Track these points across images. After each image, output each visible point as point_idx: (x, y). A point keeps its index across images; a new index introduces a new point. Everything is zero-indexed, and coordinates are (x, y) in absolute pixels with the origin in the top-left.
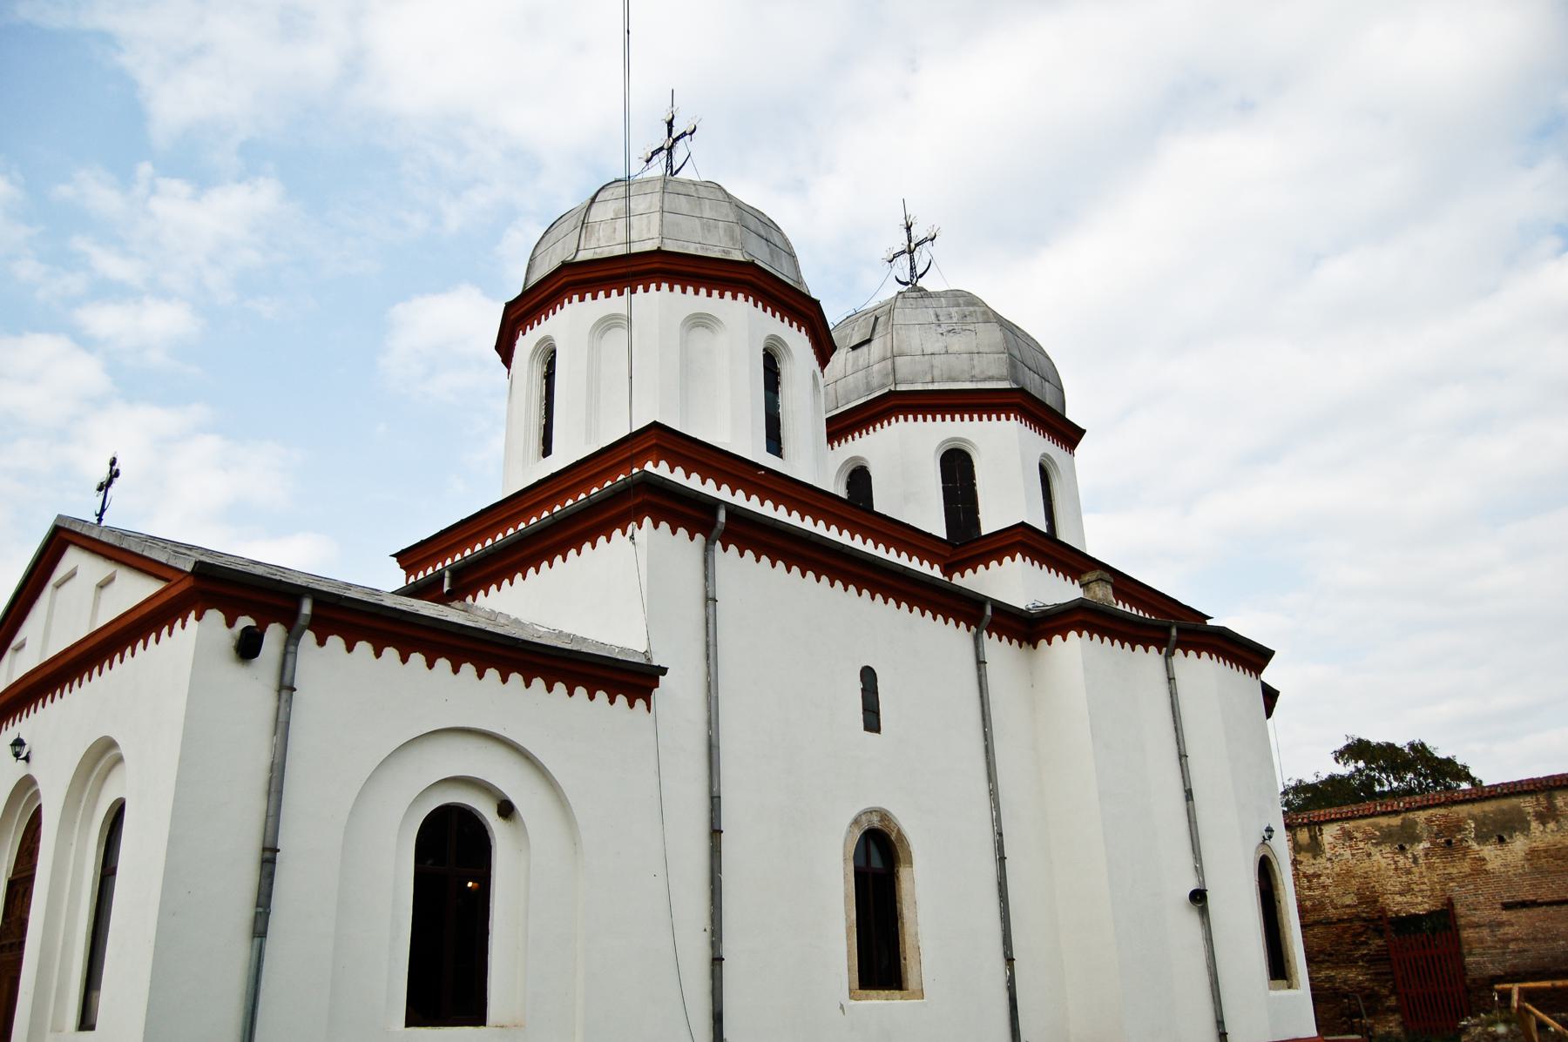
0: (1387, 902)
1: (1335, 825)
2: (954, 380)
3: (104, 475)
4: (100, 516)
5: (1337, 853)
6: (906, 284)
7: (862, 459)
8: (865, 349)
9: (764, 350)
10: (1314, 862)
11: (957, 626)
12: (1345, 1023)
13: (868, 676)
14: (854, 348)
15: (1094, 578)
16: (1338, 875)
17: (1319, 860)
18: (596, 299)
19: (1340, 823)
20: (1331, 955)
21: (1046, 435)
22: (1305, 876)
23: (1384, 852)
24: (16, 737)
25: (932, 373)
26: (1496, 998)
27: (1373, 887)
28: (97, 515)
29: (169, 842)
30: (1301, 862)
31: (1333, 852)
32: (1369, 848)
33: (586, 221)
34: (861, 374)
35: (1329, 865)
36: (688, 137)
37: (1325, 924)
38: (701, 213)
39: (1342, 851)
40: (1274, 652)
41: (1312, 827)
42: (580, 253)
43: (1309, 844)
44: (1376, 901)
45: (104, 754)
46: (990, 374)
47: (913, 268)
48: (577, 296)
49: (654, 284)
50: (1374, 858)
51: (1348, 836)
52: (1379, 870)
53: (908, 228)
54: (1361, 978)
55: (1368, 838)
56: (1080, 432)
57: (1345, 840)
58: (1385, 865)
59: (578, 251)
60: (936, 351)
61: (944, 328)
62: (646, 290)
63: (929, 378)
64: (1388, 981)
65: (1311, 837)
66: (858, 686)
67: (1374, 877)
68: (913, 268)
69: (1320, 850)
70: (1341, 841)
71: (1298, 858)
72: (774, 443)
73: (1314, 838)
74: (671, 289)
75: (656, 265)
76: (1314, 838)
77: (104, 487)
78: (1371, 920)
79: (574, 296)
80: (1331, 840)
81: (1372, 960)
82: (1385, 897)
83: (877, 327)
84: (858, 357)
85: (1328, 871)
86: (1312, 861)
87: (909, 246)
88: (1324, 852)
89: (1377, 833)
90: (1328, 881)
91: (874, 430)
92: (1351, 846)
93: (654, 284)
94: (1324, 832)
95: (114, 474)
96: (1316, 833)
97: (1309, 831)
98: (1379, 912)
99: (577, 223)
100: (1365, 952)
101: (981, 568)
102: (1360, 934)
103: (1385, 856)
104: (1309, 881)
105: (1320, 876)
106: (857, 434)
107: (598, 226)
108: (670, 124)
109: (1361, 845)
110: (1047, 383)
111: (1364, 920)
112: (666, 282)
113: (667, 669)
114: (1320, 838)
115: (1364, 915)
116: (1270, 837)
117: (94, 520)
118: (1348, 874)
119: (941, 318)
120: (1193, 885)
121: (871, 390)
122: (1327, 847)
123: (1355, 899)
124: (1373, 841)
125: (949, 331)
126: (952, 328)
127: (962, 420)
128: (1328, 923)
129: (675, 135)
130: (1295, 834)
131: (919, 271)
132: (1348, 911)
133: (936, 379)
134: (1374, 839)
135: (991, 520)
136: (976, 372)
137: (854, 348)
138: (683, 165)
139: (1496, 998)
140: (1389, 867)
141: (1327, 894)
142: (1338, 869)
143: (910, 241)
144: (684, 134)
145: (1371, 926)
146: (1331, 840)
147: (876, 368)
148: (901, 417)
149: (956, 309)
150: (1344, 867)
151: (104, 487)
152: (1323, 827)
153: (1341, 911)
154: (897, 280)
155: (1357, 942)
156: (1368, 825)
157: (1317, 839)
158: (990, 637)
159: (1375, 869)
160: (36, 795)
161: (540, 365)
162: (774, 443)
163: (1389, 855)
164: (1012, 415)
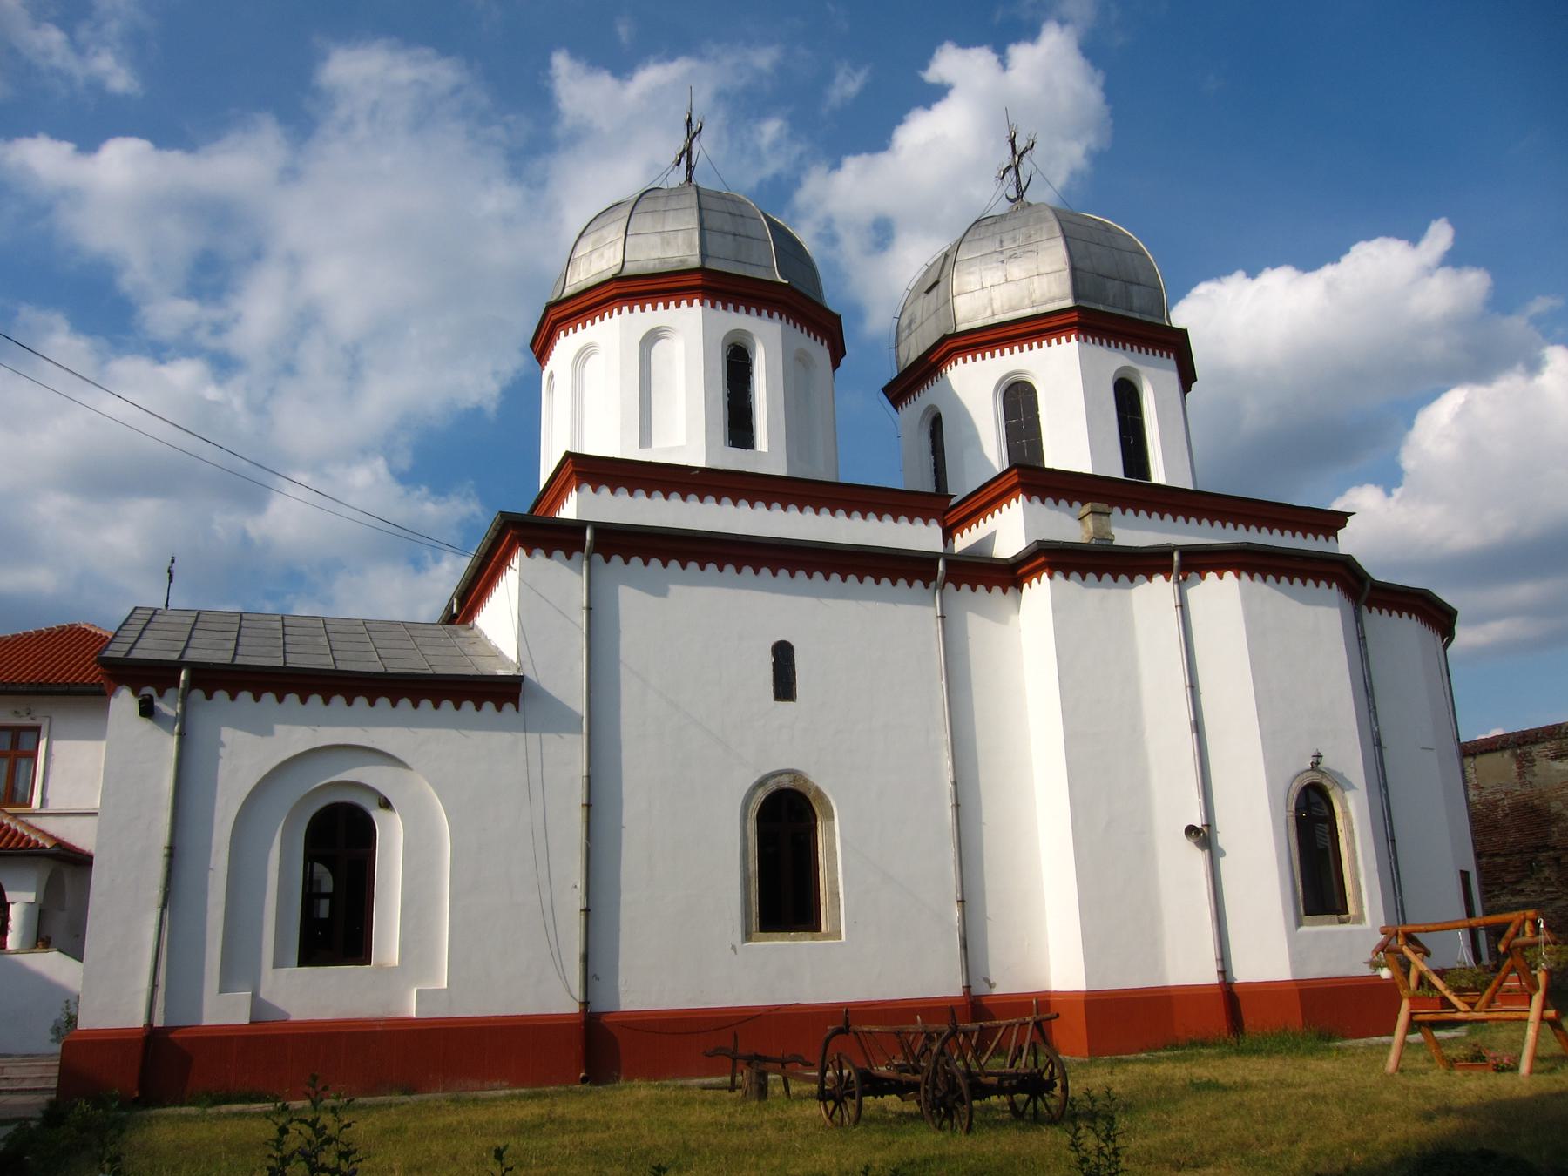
4: (167, 605)
15: (1086, 512)
26: (1542, 926)
36: (1028, 152)
46: (1052, 295)
63: (989, 312)
66: (769, 660)
68: (1018, 183)
75: (614, 292)
79: (624, 308)
108: (1013, 142)
110: (1135, 288)
116: (1318, 763)
117: (164, 607)
139: (1542, 926)
143: (1014, 152)
164: (1073, 336)
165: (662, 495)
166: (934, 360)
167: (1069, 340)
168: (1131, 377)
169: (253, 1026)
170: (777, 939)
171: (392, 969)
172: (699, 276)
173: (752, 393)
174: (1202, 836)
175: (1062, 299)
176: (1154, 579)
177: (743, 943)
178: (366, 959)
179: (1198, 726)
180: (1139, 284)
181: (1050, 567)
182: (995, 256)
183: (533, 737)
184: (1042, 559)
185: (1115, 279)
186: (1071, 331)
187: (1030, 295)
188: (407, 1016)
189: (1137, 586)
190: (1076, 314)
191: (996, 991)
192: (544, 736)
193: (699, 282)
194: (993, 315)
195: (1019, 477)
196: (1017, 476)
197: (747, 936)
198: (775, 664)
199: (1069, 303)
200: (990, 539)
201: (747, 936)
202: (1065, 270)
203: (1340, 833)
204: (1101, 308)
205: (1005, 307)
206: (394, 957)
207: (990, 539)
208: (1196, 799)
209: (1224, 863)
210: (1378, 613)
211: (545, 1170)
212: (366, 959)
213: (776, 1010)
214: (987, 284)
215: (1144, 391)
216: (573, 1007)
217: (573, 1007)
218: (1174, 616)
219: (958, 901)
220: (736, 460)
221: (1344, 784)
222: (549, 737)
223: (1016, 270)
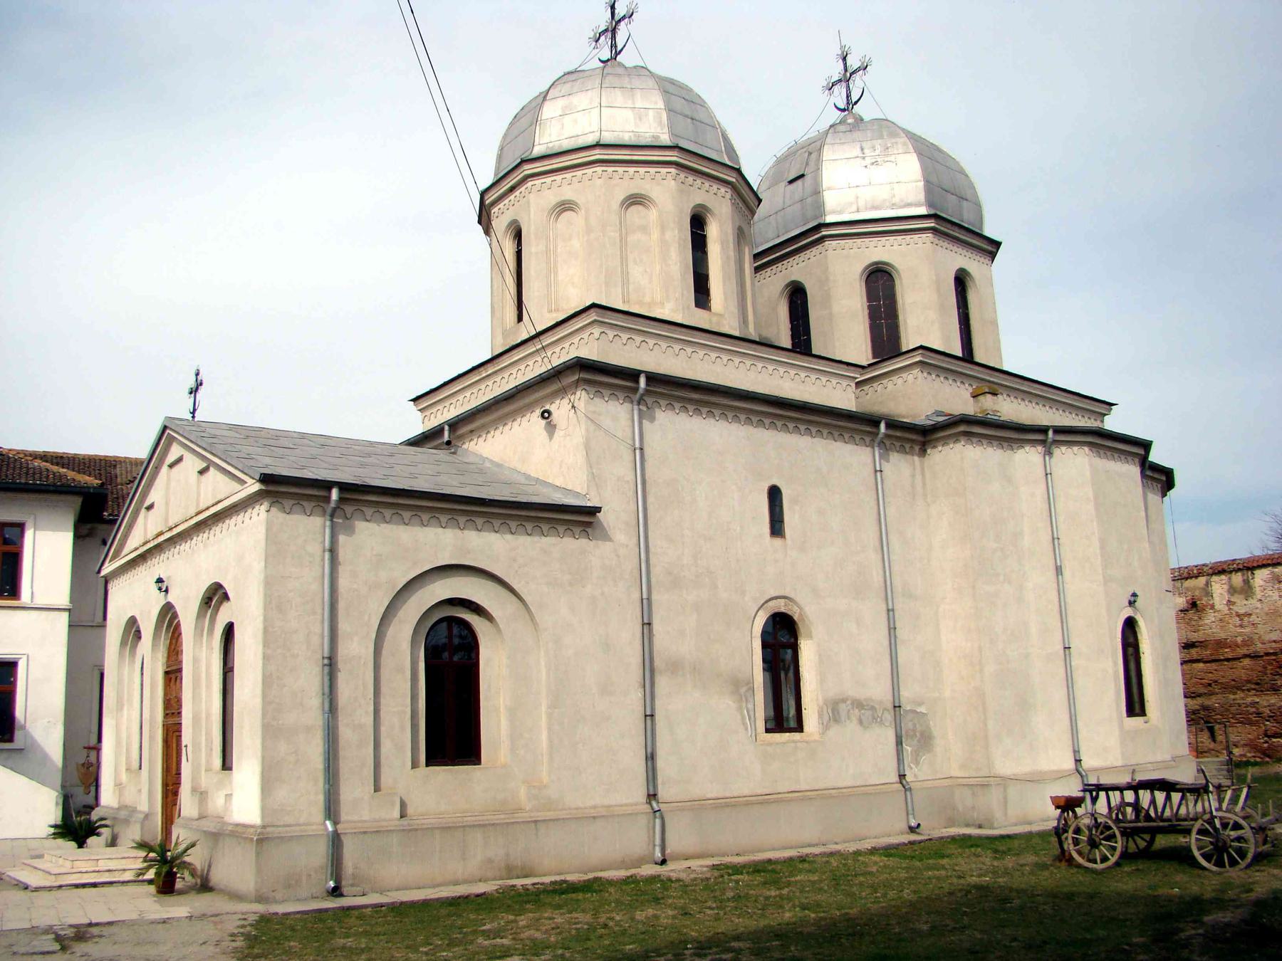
3: (191, 383)
5: (1267, 595)
6: (843, 110)
8: (799, 182)
10: (1246, 602)
14: (791, 182)
16: (1267, 614)
17: (1251, 601)
19: (1270, 568)
22: (1238, 615)
24: (158, 577)
25: (857, 204)
28: (191, 413)
29: (263, 683)
30: (1234, 603)
31: (1263, 594)
33: (539, 119)
34: (797, 207)
35: (1259, 605)
36: (627, 20)
38: (634, 103)
40: (1152, 442)
43: (1242, 587)
45: (215, 596)
46: (909, 201)
47: (848, 96)
53: (844, 59)
56: (997, 244)
57: (1274, 584)
61: (868, 161)
63: (854, 208)
65: (1244, 580)
68: (848, 96)
70: (1270, 584)
73: (1246, 582)
76: (1246, 582)
77: (194, 391)
80: (1262, 583)
85: (1258, 611)
87: (845, 74)
88: (1254, 594)
90: (1257, 621)
94: (1256, 576)
95: (199, 384)
96: (1248, 577)
97: (1243, 575)
104: (1241, 620)
105: (1250, 615)
107: (549, 123)
108: (613, 7)
113: (601, 508)
114: (1252, 581)
117: (189, 417)
119: (866, 151)
122: (1258, 590)
125: (873, 164)
126: (875, 160)
129: (617, 18)
130: (1230, 579)
131: (854, 99)
132: (1274, 645)
136: (896, 200)
137: (791, 182)
138: (624, 46)
143: (846, 70)
144: (623, 18)
146: (1262, 583)
147: (809, 200)
149: (879, 141)
151: (194, 391)
152: (1254, 572)
153: (1268, 645)
154: (836, 107)
157: (1249, 582)
160: (175, 616)
161: (511, 242)
168: (961, 277)
175: (918, 205)
180: (966, 200)
185: (953, 194)
202: (921, 181)
205: (869, 206)
211: (829, 958)
212: (802, 732)
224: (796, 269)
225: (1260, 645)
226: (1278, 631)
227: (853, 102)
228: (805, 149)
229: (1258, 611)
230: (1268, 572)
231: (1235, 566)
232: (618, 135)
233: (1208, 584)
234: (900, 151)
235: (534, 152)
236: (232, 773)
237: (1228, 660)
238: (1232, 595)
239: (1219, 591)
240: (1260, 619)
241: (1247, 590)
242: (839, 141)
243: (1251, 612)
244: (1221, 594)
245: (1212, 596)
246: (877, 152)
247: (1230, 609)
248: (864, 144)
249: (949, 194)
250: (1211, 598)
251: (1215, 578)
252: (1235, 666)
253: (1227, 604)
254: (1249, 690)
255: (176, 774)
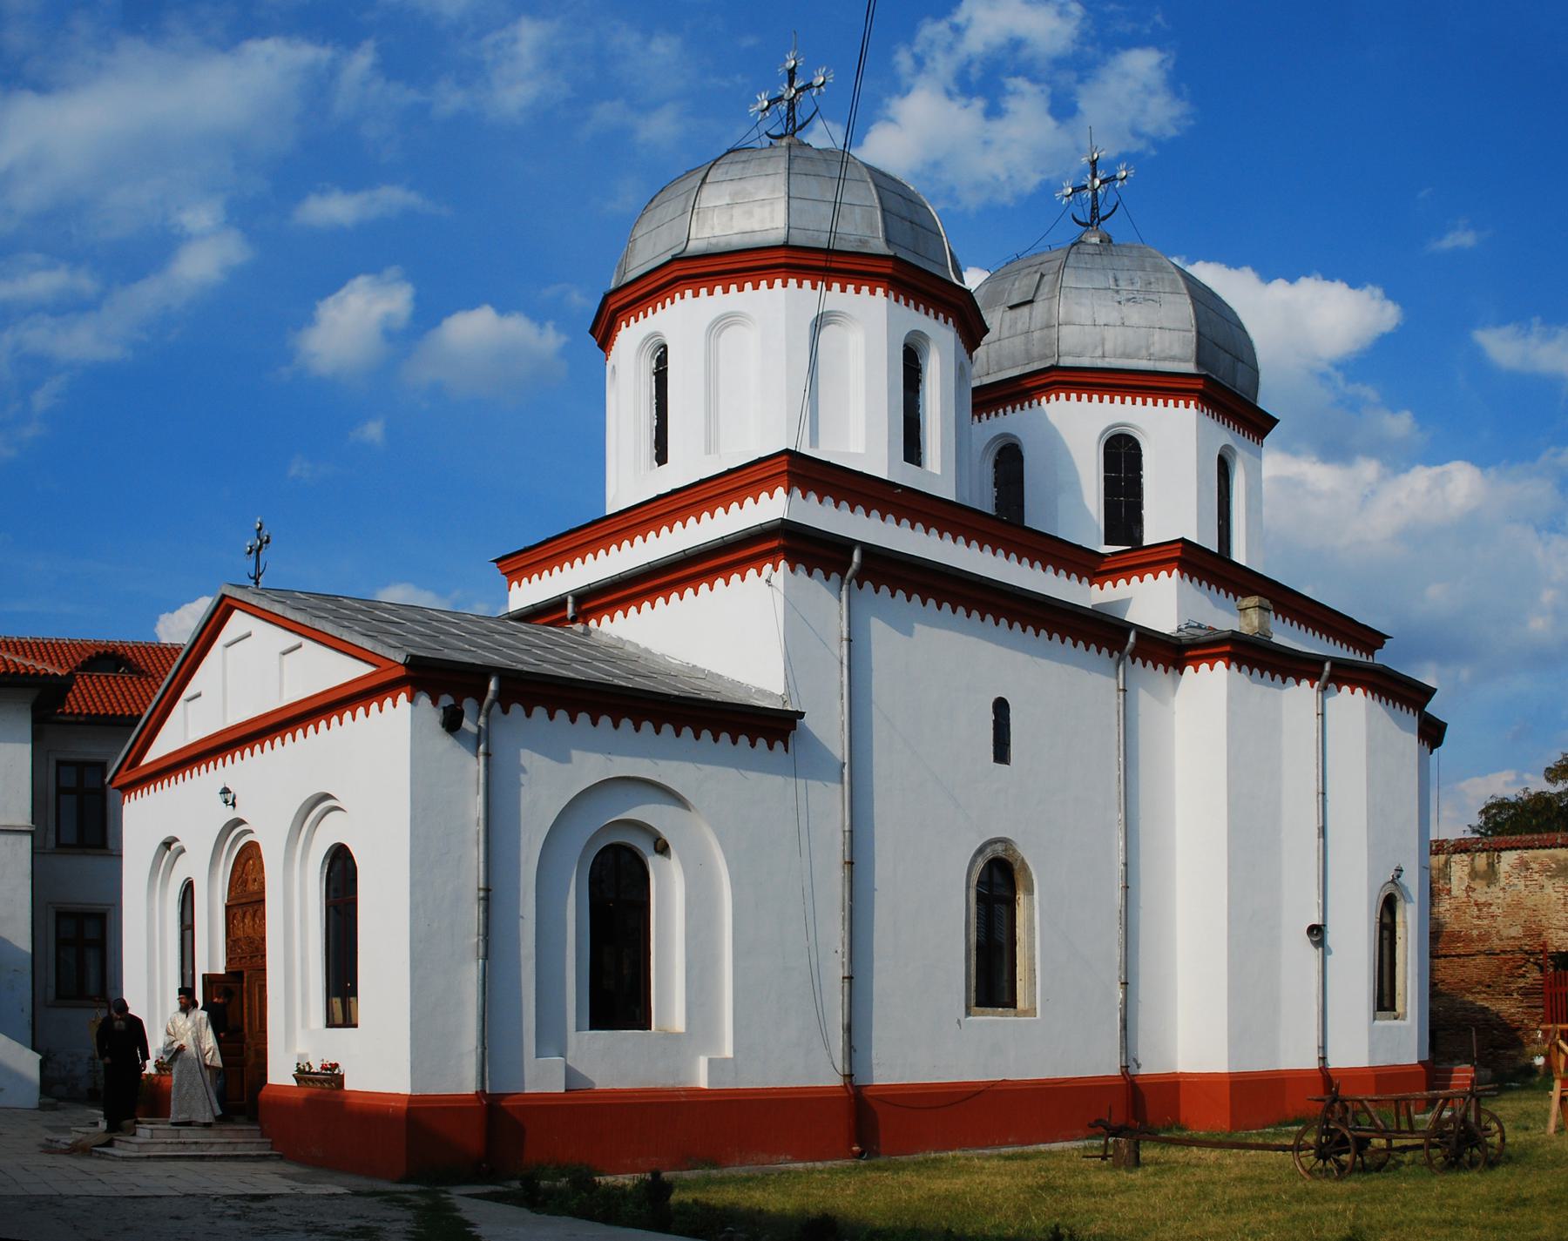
0: (1551, 936)
1: (1514, 852)
2: (1128, 356)
5: (1511, 883)
7: (1015, 437)
8: (1025, 310)
9: (905, 345)
10: (1488, 890)
11: (1099, 652)
12: (1490, 1054)
13: (1001, 707)
14: (1011, 308)
15: (1252, 605)
18: (712, 294)
19: (1519, 851)
20: (1489, 986)
21: (1231, 423)
23: (1556, 885)
27: (1540, 921)
32: (1543, 880)
37: (1488, 954)
39: (1516, 881)
41: (1491, 853)
42: (690, 242)
43: (1485, 872)
44: (1540, 935)
46: (1173, 353)
48: (690, 291)
49: (780, 280)
50: (1546, 891)
51: (1524, 865)
52: (1548, 904)
54: (1513, 1010)
55: (1544, 870)
58: (1555, 899)
59: (688, 240)
60: (1111, 322)
61: (1124, 296)
62: (770, 286)
63: (1099, 352)
64: (1538, 1014)
65: (1488, 864)
66: (990, 717)
67: (1543, 910)
69: (1495, 879)
70: (1517, 871)
71: (1472, 885)
72: (913, 450)
73: (1491, 865)
74: (800, 285)
76: (1491, 865)
78: (1532, 954)
81: (1526, 993)
82: (1550, 931)
83: (1041, 287)
84: (1017, 318)
85: (1499, 901)
86: (1486, 889)
88: (1498, 880)
89: (1553, 865)
91: (1030, 406)
92: (1525, 877)
93: (780, 280)
94: (1502, 860)
97: (1488, 857)
98: (1542, 945)
99: (685, 208)
100: (1522, 985)
101: (1135, 579)
102: (1520, 967)
103: (1557, 890)
104: (1479, 910)
105: (1491, 904)
106: (1009, 408)
109: (1536, 876)
110: (1240, 364)
111: (1526, 952)
112: (793, 278)
115: (1527, 948)
116: (1399, 877)
118: (1518, 905)
119: (1121, 283)
120: (1316, 920)
121: (1030, 361)
122: (1502, 876)
123: (1521, 931)
124: (1548, 874)
125: (1129, 300)
126: (1132, 296)
127: (1134, 403)
128: (1491, 953)
130: (1473, 860)
132: (1511, 942)
133: (1107, 354)
134: (1550, 871)
135: (1154, 532)
136: (1155, 349)
137: (1011, 308)
140: (1559, 901)
141: (1494, 925)
142: (1510, 899)
145: (1532, 960)
147: (1037, 335)
148: (1063, 395)
149: (1139, 273)
150: (1516, 898)
152: (1501, 854)
153: (1506, 942)
155: (1516, 974)
156: (1547, 856)
157: (1493, 866)
158: (1133, 663)
159: (1545, 902)
162: (913, 450)
163: (1561, 889)
164: (1192, 403)
165: (863, 510)
166: (1028, 386)
167: (1187, 406)
169: (569, 1095)
170: (988, 1015)
171: (679, 1034)
172: (890, 264)
173: (921, 403)
174: (1317, 933)
176: (1301, 684)
177: (966, 1017)
178: (645, 1024)
179: (1323, 832)
180: (1243, 362)
181: (1229, 657)
182: (1110, 293)
183: (801, 782)
184: (1228, 648)
185: (1226, 352)
186: (1191, 398)
187: (1148, 348)
188: (694, 1086)
189: (1289, 687)
190: (1202, 382)
191: (1142, 1071)
192: (809, 782)
193: (889, 271)
194: (1104, 356)
195: (1181, 552)
196: (1180, 550)
197: (968, 1013)
198: (995, 722)
199: (1190, 367)
200: (1125, 603)
201: (968, 1013)
202: (1190, 331)
203: (1398, 940)
204: (1214, 377)
206: (679, 1024)
207: (1125, 603)
208: (1315, 899)
209: (1329, 958)
210: (1236, 670)
213: (993, 1085)
214: (1101, 321)
215: (1236, 473)
216: (836, 1081)
217: (836, 1081)
218: (1314, 722)
219: (1122, 984)
220: (907, 476)
221: (1408, 899)
222: (815, 785)
223: (1135, 314)
224: (1010, 421)
225: (1496, 941)
226: (1519, 926)
227: (1100, 217)
228: (1035, 268)
229: (1499, 901)
230: (1517, 857)
231: (1480, 845)
232: (813, 235)
233: (1447, 863)
234: (1167, 290)
235: (688, 248)
236: (1176, 683)
237: (1459, 956)
238: (1473, 880)
239: (1459, 874)
240: (1500, 911)
241: (1490, 875)
242: (1084, 266)
243: (1491, 902)
244: (1461, 878)
245: (1450, 879)
246: (1137, 287)
247: (1468, 896)
248: (1119, 274)
249: (1222, 351)
250: (1448, 881)
251: (1456, 857)
252: (1466, 964)
253: (1466, 890)
254: (1479, 993)
255: (259, 1031)
